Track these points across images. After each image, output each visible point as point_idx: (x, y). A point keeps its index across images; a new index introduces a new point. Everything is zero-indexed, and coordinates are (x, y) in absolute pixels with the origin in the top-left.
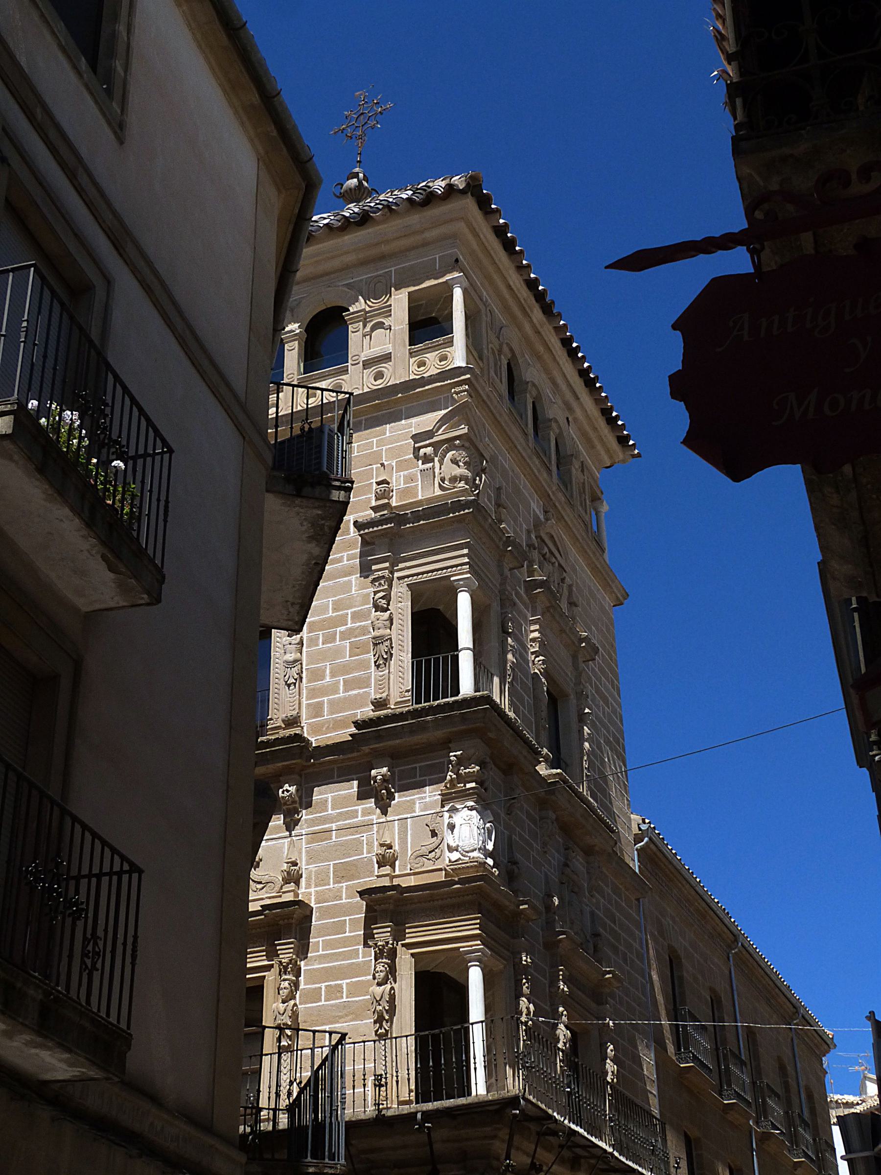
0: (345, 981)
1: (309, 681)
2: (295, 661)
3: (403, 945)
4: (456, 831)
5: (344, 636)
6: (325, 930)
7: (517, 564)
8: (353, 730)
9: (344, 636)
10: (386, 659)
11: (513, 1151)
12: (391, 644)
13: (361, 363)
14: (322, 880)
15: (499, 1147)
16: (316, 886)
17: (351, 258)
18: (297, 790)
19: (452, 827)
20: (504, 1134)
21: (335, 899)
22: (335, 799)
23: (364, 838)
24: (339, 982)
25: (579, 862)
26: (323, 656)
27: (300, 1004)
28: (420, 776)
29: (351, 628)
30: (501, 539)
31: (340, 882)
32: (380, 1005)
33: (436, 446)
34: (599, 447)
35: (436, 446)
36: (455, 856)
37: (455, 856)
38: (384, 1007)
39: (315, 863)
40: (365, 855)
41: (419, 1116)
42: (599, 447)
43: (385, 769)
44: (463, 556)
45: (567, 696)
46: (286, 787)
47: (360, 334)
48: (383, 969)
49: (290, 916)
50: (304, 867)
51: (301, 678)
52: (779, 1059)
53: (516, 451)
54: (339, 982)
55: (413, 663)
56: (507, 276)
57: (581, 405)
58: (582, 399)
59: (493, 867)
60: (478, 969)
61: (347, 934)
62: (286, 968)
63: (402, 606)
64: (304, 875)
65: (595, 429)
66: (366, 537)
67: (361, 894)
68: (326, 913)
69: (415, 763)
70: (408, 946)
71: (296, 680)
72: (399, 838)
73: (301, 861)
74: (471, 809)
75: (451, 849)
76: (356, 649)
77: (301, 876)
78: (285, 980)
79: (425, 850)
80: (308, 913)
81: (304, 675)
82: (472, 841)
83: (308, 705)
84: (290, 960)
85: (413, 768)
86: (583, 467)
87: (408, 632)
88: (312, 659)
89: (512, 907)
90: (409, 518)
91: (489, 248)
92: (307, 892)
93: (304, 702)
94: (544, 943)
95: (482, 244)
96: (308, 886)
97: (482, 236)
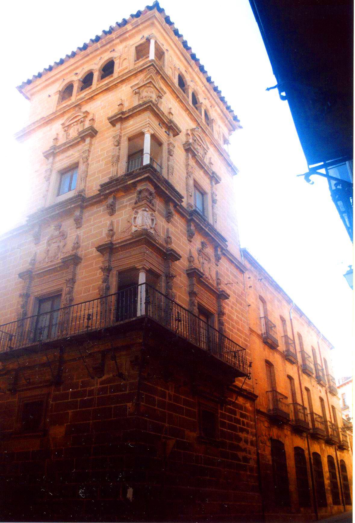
25: (209, 250)
52: (312, 347)
86: (219, 127)
92: (81, 253)
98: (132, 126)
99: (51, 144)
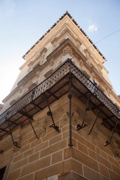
65: (99, 55)
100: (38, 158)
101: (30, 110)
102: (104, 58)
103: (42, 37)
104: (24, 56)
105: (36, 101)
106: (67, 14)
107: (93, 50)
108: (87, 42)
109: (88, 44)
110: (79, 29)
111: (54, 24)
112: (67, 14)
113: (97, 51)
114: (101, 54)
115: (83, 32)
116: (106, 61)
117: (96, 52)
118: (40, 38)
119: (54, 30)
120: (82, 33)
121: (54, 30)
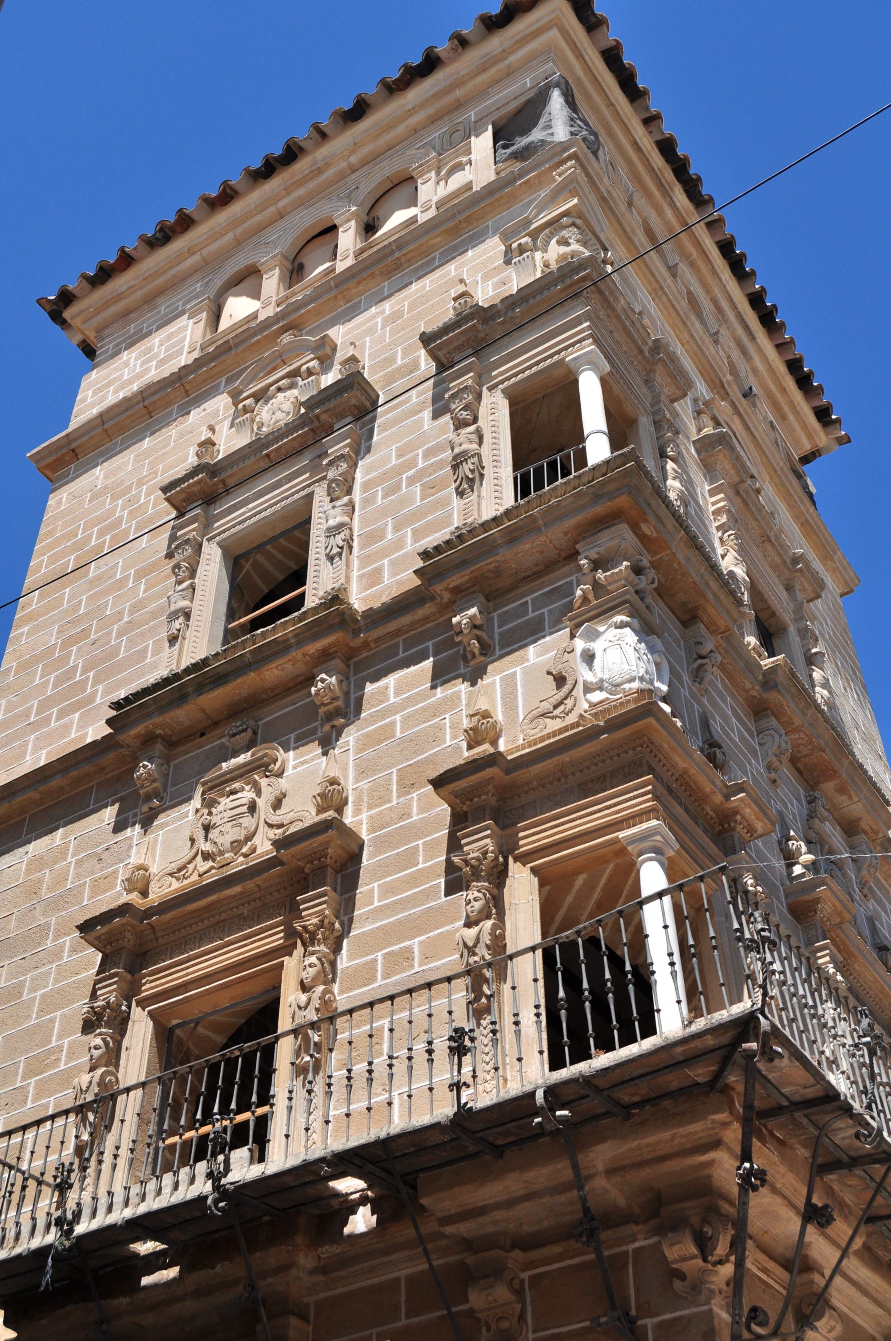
0: (416, 940)
1: (362, 547)
2: (340, 526)
3: (516, 859)
4: (597, 662)
5: (411, 481)
6: (383, 869)
7: (679, 393)
8: (420, 564)
9: (411, 481)
10: (472, 480)
11: (756, 1144)
12: (480, 461)
13: (434, 206)
14: (379, 796)
15: (725, 1169)
16: (370, 808)
17: (419, 117)
18: (340, 682)
19: (589, 658)
20: (733, 1134)
21: (401, 818)
22: (400, 695)
23: (447, 721)
24: (407, 943)
26: (383, 513)
27: (341, 992)
28: (533, 611)
29: (422, 469)
30: (645, 343)
31: (409, 793)
32: (475, 954)
33: (534, 235)
34: (791, 418)
35: (534, 235)
36: (596, 696)
37: (596, 696)
38: (483, 958)
39: (368, 776)
40: (448, 743)
41: (540, 1095)
42: (791, 418)
43: (473, 611)
44: (582, 331)
45: (784, 630)
46: (324, 676)
47: (431, 183)
48: (480, 895)
49: (319, 854)
50: (351, 787)
51: (351, 548)
53: (664, 299)
54: (407, 943)
55: (515, 479)
56: (629, 125)
57: (760, 350)
58: (758, 340)
59: (665, 699)
60: (655, 864)
61: (420, 866)
62: (313, 935)
63: (496, 413)
64: (350, 799)
65: (784, 390)
66: (440, 354)
67: (438, 783)
68: (381, 844)
69: (524, 596)
70: (523, 859)
71: (342, 548)
72: (504, 704)
73: (346, 777)
74: (622, 625)
75: (588, 689)
76: (430, 488)
77: (346, 802)
78: (313, 953)
79: (547, 706)
80: (355, 849)
81: (355, 544)
82: (626, 667)
83: (361, 577)
84: (322, 921)
85: (522, 604)
87: (506, 457)
88: (364, 522)
89: (718, 799)
90: (499, 312)
91: (600, 79)
93: (355, 574)
94: (788, 905)
95: (588, 69)
96: (357, 811)
97: (587, 58)
98: (522, 362)
99: (192, 461)
100: (29, 1017)
101: (413, 1149)
102: (823, 414)
103: (278, 151)
104: (66, 298)
105: (827, 1140)
106: (38, 301)
107: (745, 339)
108: (700, 263)
109: (710, 280)
110: (647, 143)
111: (416, 60)
112: (38, 301)
113: (778, 346)
114: (804, 382)
115: (680, 168)
116: (844, 441)
117: (765, 359)
118: (256, 164)
119: (411, 112)
120: (669, 175)
121: (411, 112)
